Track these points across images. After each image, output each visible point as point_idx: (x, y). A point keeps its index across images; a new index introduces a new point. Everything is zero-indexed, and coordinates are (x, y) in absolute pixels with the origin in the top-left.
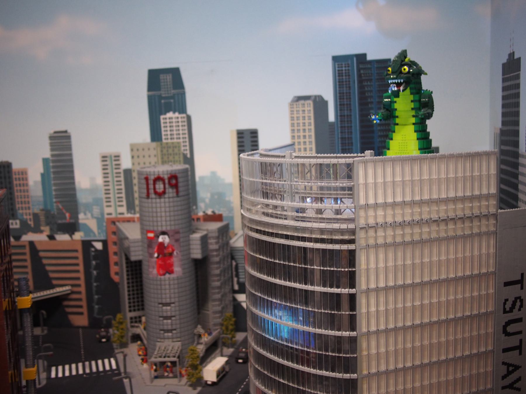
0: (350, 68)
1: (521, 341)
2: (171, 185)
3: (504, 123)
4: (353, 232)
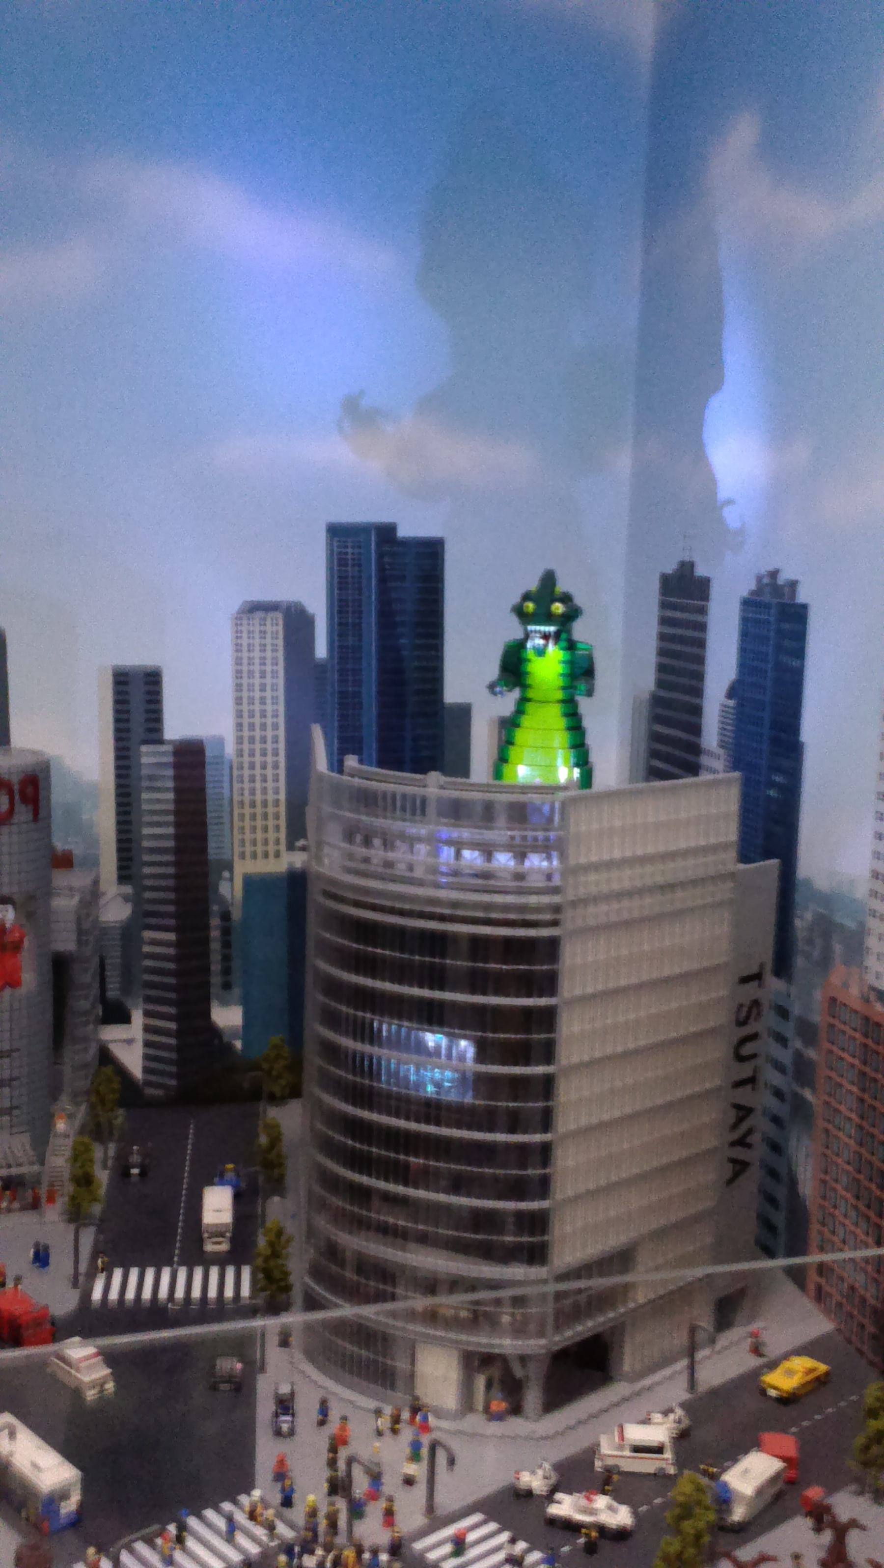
2: (24, 800)
3: (661, 684)
4: (557, 909)
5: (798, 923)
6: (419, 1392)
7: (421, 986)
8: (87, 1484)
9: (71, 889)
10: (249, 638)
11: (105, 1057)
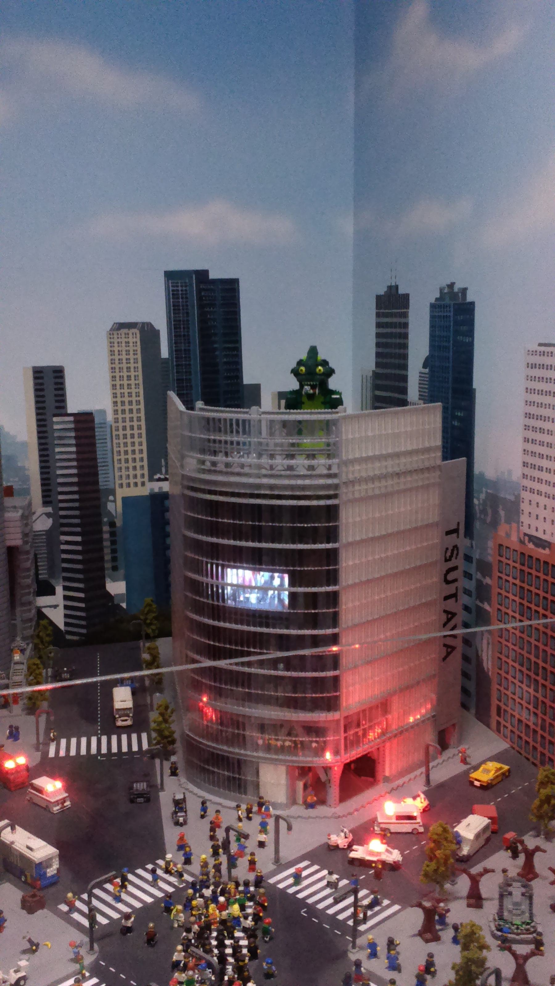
0: (188, 288)
1: (457, 588)
3: (378, 365)
5: (476, 501)
6: (262, 794)
7: (253, 541)
8: (62, 857)
9: (15, 507)
10: (119, 346)
11: (41, 615)
